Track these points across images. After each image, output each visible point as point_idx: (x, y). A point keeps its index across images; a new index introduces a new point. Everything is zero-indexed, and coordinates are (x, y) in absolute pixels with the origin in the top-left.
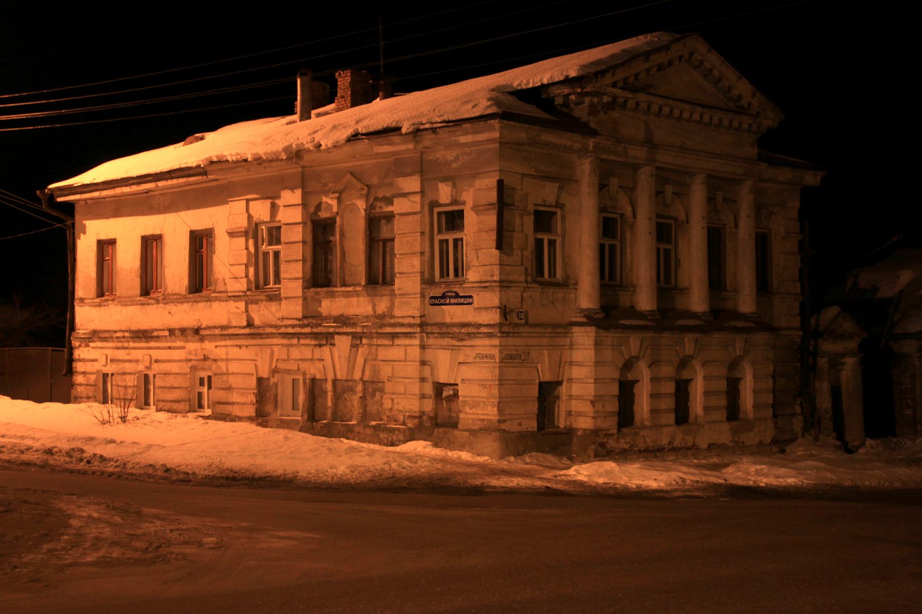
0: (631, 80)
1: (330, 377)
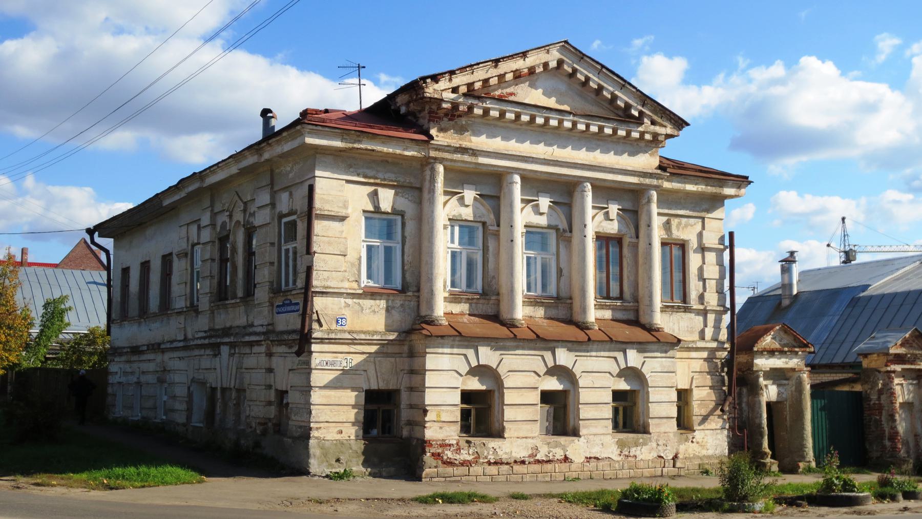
0: (478, 85)
1: (219, 386)
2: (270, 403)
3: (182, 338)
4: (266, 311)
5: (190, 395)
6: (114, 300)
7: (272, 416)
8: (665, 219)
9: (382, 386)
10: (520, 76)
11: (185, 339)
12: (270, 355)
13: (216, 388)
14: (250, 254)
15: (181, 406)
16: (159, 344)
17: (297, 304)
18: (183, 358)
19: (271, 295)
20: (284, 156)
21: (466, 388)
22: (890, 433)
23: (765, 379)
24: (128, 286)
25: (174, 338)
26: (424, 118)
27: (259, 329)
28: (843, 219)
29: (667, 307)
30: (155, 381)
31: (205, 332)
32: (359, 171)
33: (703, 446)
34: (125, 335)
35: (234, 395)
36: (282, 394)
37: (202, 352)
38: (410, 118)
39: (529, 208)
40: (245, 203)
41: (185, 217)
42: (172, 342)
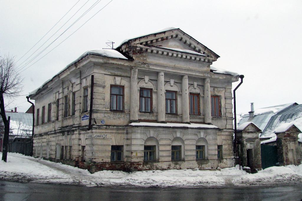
0: (149, 42)
2: (80, 150)
3: (54, 130)
4: (78, 119)
5: (56, 149)
6: (35, 119)
7: (80, 155)
8: (212, 88)
9: (117, 144)
10: (163, 40)
11: (55, 131)
12: (80, 134)
13: (64, 146)
14: (74, 101)
15: (53, 153)
16: (47, 133)
17: (88, 116)
18: (54, 137)
19: (80, 114)
20: (83, 66)
21: (146, 145)
22: (286, 159)
23: (246, 142)
24: (39, 115)
25: (52, 130)
26: (131, 53)
27: (77, 125)
28: (252, 104)
29: (214, 117)
30: (46, 145)
31: (60, 128)
32: (109, 71)
33: (226, 164)
34: (38, 130)
35: (69, 148)
36: (83, 147)
37: (59, 134)
38: (126, 54)
39: (168, 84)
40: (73, 84)
41: (55, 91)
42: (51, 132)
